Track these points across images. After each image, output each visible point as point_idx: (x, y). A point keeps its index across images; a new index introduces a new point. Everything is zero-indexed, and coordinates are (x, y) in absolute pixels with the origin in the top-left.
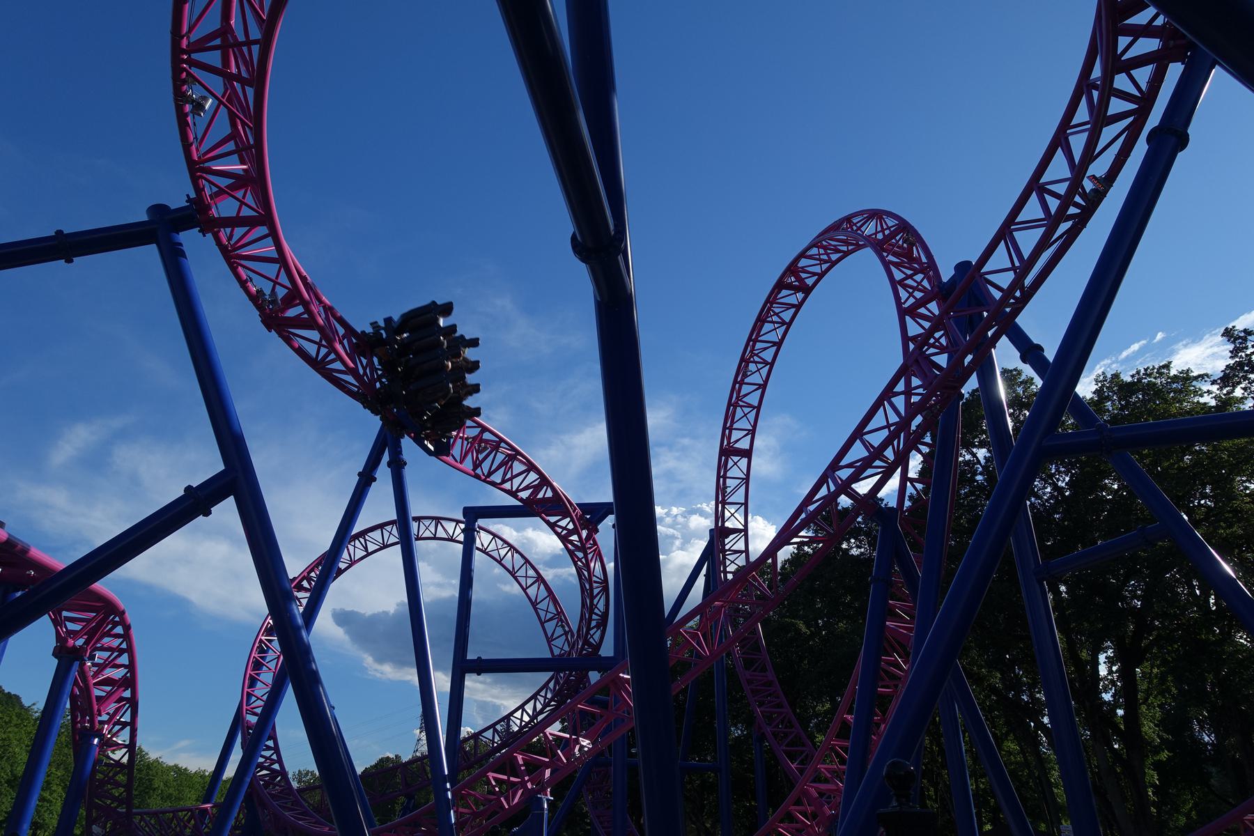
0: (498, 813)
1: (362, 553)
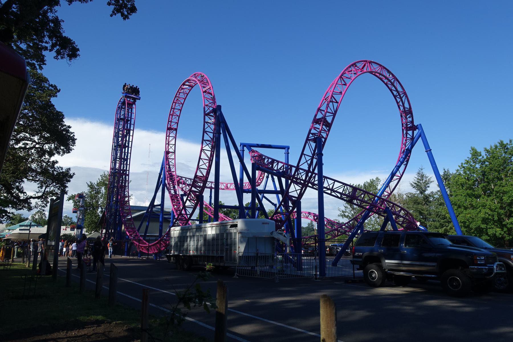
1: (173, 161)
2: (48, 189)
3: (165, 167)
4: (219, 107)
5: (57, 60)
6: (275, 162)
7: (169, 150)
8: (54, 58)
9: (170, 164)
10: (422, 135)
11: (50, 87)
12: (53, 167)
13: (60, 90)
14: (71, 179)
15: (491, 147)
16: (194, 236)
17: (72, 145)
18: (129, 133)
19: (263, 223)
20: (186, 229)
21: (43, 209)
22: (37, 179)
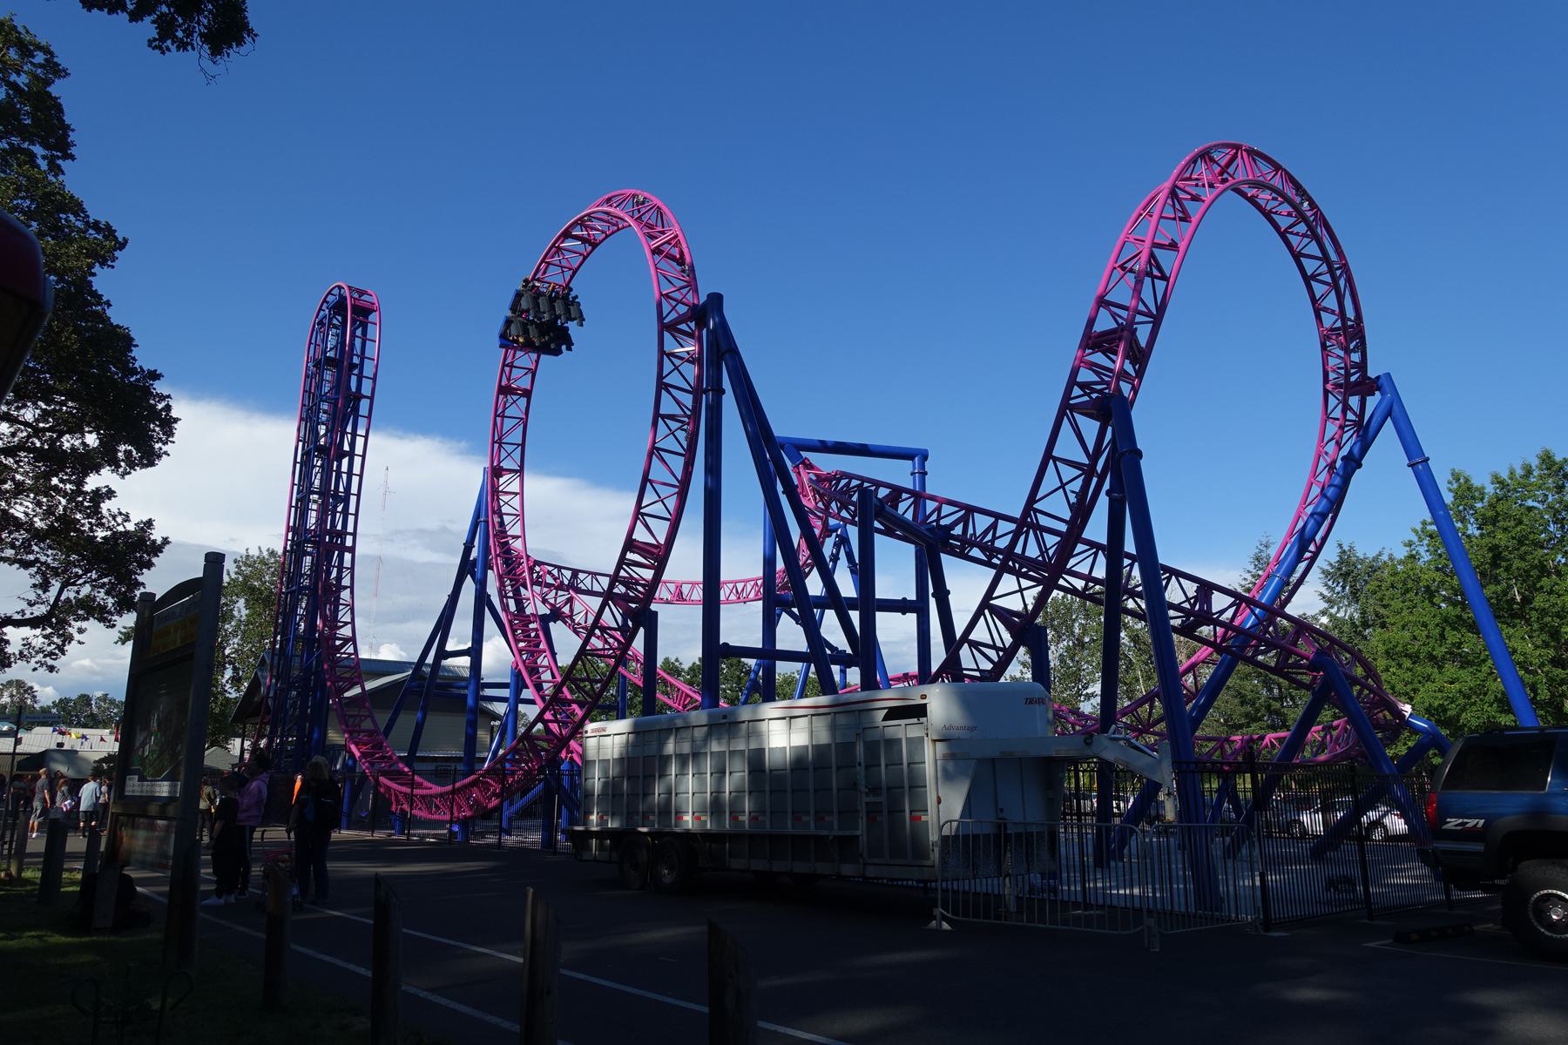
0: (338, 399)
1: (516, 502)
2: (70, 594)
3: (487, 522)
4: (716, 300)
5: (163, 53)
6: (905, 496)
7: (501, 465)
8: (150, 46)
9: (505, 509)
10: (1394, 411)
11: (91, 231)
12: (95, 511)
13: (126, 241)
14: (154, 560)
15: (1512, 473)
16: (696, 755)
17: (160, 440)
18: (356, 409)
19: (1030, 701)
20: (658, 728)
21: (49, 661)
22: (31, 557)
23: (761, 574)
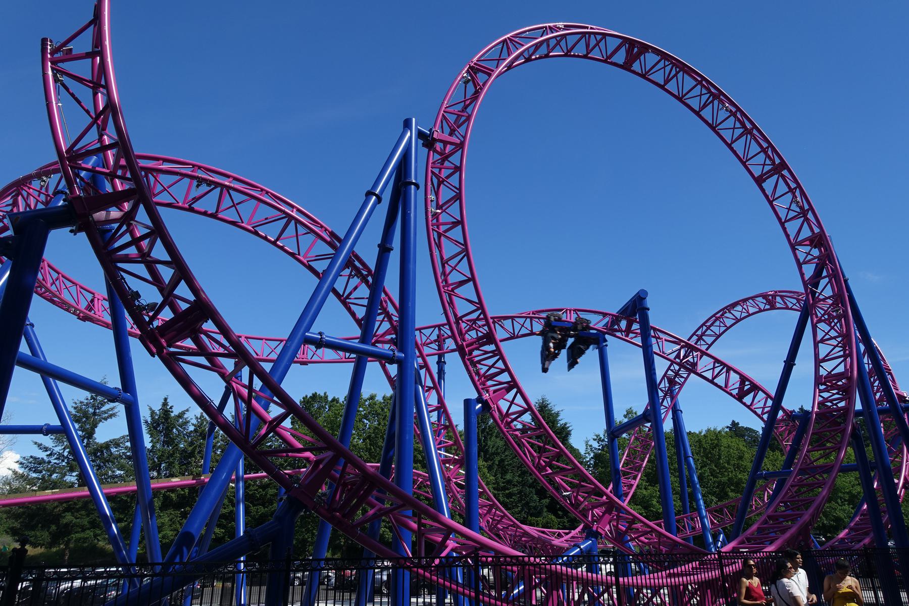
23: (127, 433)
